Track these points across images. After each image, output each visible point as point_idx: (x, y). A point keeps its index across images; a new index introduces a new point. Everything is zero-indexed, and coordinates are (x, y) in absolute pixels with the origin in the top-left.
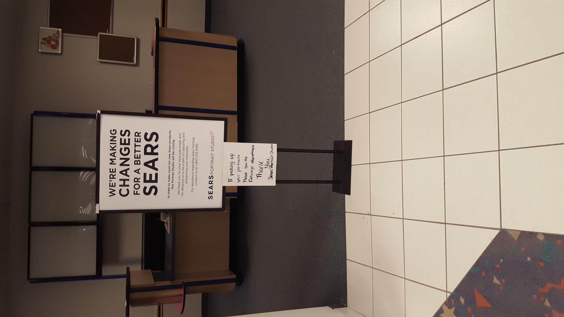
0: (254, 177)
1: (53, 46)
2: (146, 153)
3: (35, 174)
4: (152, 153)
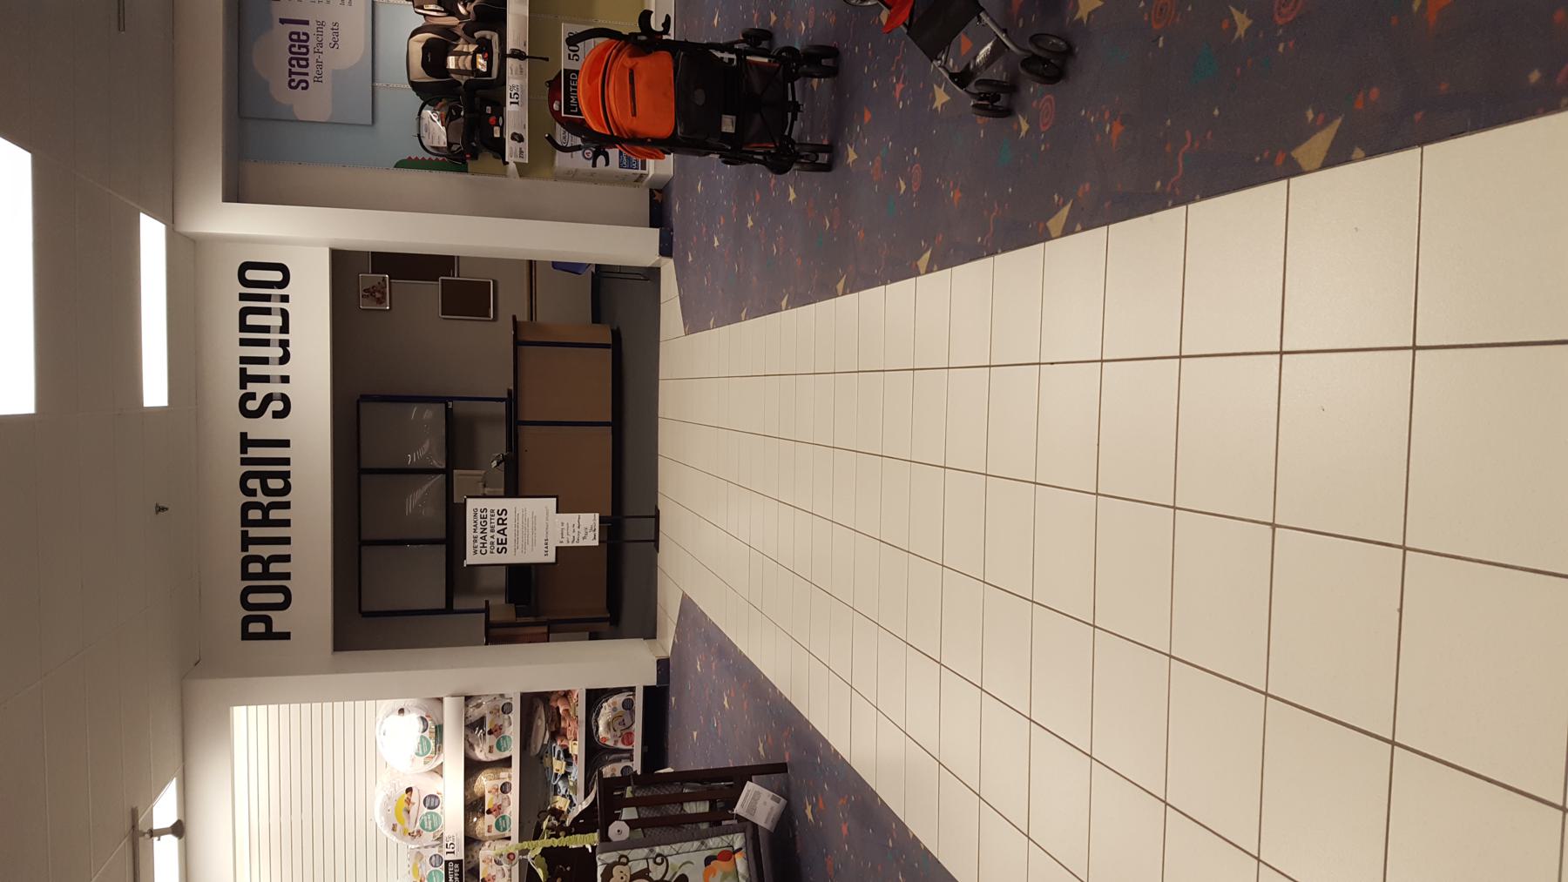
0: (581, 539)
1: (378, 299)
2: (498, 524)
3: (364, 477)
4: (503, 524)
